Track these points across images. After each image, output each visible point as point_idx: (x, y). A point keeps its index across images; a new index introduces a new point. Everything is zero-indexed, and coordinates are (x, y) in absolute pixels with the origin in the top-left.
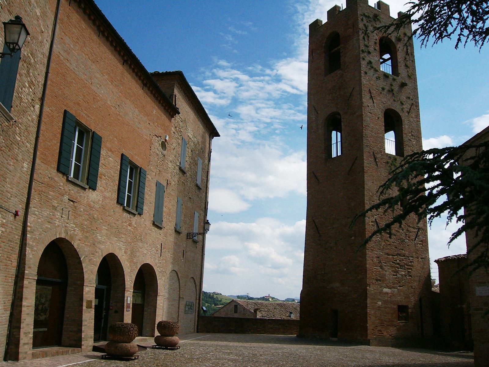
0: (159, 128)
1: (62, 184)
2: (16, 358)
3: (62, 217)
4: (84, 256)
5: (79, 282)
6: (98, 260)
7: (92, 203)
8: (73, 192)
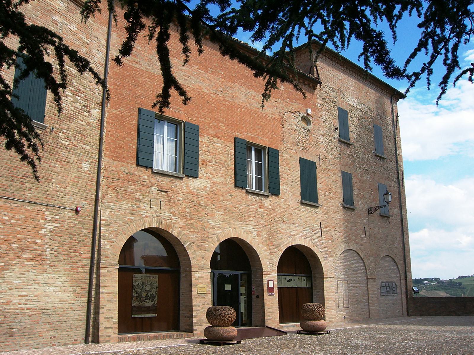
0: (294, 104)
1: (146, 177)
2: (96, 340)
3: (150, 207)
4: (189, 243)
5: (188, 269)
6: (213, 246)
7: (195, 191)
8: (164, 183)
